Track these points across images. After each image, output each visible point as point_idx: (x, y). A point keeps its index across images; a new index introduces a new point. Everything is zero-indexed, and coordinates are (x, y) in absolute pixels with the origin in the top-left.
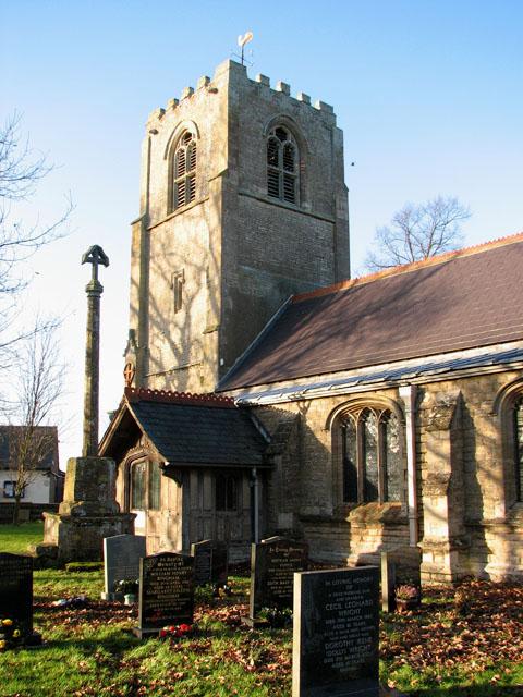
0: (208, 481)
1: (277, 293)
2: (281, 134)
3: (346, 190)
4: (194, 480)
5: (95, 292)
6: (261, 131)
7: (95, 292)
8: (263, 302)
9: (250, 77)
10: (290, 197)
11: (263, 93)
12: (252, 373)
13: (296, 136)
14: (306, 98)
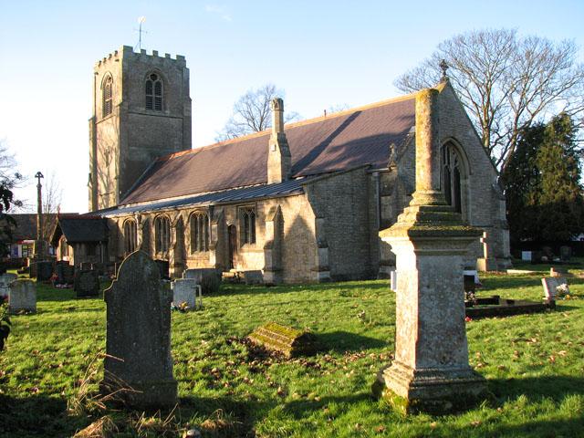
0: (83, 246)
1: (149, 158)
2: (154, 77)
3: (191, 100)
4: (78, 246)
5: (39, 187)
6: (142, 78)
7: (39, 187)
8: (142, 163)
9: (135, 51)
10: (159, 108)
11: (143, 59)
12: (127, 200)
13: (162, 77)
14: (168, 55)
